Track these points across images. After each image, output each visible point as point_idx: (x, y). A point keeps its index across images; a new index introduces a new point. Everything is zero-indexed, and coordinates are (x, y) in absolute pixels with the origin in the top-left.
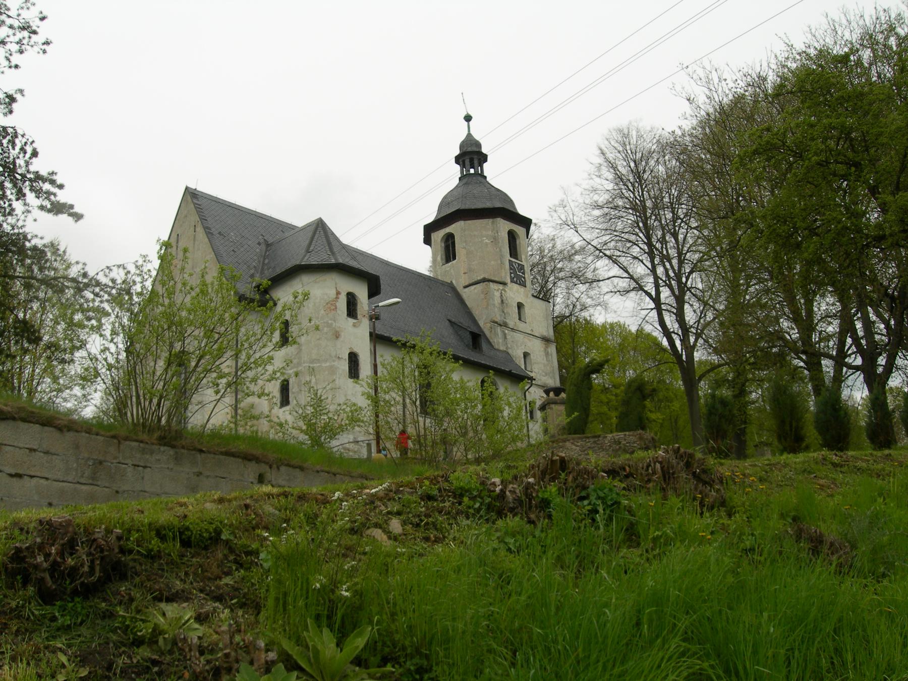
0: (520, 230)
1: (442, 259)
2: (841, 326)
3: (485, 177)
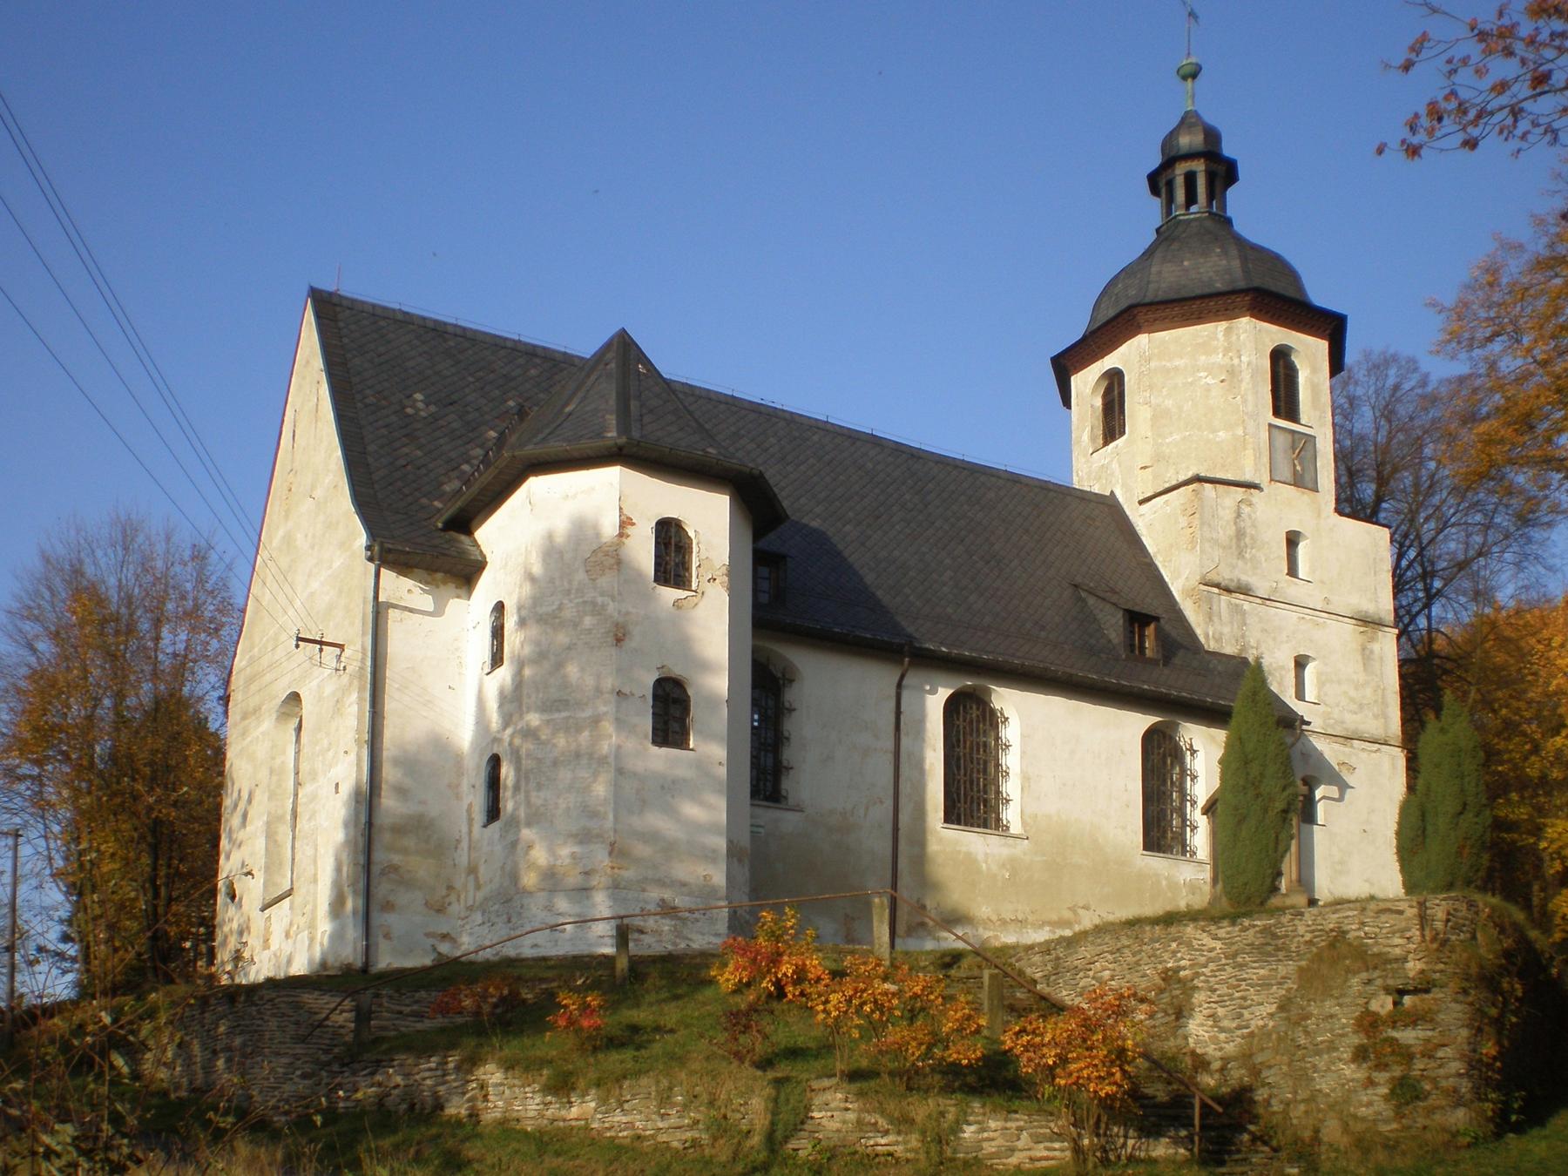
0: (1310, 353)
1: (1093, 439)
2: (78, 984)
3: (1229, 222)
